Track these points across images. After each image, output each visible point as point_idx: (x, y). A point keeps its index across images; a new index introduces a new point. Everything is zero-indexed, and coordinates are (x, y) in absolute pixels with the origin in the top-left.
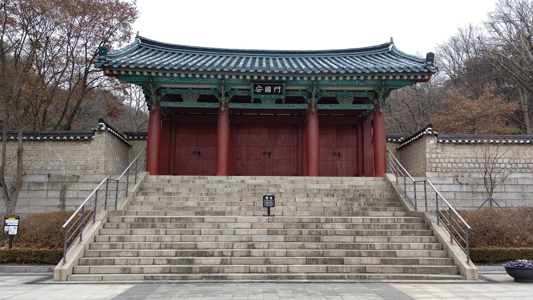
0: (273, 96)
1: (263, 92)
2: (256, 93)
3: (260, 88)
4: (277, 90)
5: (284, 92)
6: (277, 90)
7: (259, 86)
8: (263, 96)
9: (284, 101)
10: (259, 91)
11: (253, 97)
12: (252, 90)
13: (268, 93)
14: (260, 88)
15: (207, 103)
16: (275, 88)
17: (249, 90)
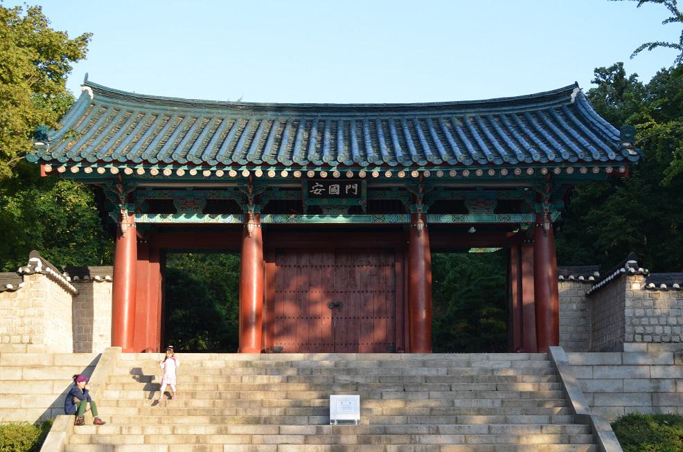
0: (344, 202)
1: (325, 194)
2: (312, 196)
3: (319, 188)
4: (351, 190)
5: (364, 192)
6: (351, 190)
7: (318, 185)
8: (325, 202)
9: (364, 210)
10: (317, 192)
11: (307, 203)
12: (305, 191)
13: (335, 196)
14: (319, 188)
15: (387, 216)
16: (348, 187)
17: (299, 189)
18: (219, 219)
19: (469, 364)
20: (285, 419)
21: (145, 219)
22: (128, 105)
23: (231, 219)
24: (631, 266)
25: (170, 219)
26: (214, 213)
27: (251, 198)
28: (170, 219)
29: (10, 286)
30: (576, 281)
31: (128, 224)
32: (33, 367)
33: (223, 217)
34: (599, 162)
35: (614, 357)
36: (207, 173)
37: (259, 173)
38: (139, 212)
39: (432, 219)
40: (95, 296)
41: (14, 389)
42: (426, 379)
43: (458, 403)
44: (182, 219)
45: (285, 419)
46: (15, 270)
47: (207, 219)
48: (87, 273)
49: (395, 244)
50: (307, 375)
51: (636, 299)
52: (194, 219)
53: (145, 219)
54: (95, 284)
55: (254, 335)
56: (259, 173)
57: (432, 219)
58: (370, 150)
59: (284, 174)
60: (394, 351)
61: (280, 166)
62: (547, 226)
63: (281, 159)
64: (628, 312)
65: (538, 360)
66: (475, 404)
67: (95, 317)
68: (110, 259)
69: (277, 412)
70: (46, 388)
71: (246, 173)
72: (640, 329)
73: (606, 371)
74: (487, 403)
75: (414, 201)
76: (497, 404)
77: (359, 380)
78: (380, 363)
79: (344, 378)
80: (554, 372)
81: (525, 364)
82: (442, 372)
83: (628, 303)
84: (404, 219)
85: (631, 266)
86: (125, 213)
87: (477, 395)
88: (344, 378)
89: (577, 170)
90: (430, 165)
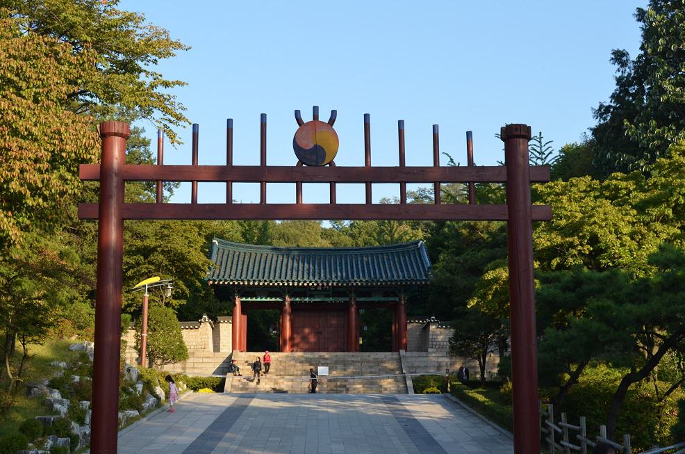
0: (323, 293)
11: (308, 293)
18: (273, 299)
19: (369, 356)
20: (302, 375)
21: (244, 299)
22: (277, 261)
23: (278, 299)
24: (433, 319)
25: (254, 299)
26: (271, 297)
27: (286, 291)
28: (254, 299)
29: (196, 327)
30: (419, 322)
31: (238, 301)
32: (207, 357)
33: (261, 298)
34: (419, 280)
35: (424, 354)
36: (271, 284)
37: (291, 284)
38: (242, 297)
39: (358, 299)
40: (221, 329)
41: (200, 366)
42: (353, 361)
43: (363, 370)
44: (259, 299)
45: (302, 375)
46: (198, 321)
47: (268, 299)
48: (217, 319)
49: (345, 308)
50: (309, 361)
51: (433, 332)
52: (264, 299)
53: (244, 299)
54: (221, 324)
55: (288, 347)
56: (291, 284)
57: (358, 299)
58: (328, 276)
59: (300, 284)
60: (344, 352)
61: (299, 282)
62: (403, 302)
63: (299, 279)
64: (430, 337)
65: (395, 355)
66: (369, 370)
67: (221, 337)
68: (231, 314)
69: (299, 373)
70: (212, 365)
71: (286, 284)
72: (435, 343)
73: (421, 359)
74: (374, 370)
75: (351, 292)
76: (377, 370)
77: (328, 362)
78: (336, 356)
79: (323, 361)
80: (399, 360)
81: (390, 356)
82: (359, 359)
83: (430, 333)
84: (347, 299)
85: (433, 319)
86: (237, 297)
87: (370, 367)
88: (323, 361)
89: (411, 283)
90: (361, 281)
